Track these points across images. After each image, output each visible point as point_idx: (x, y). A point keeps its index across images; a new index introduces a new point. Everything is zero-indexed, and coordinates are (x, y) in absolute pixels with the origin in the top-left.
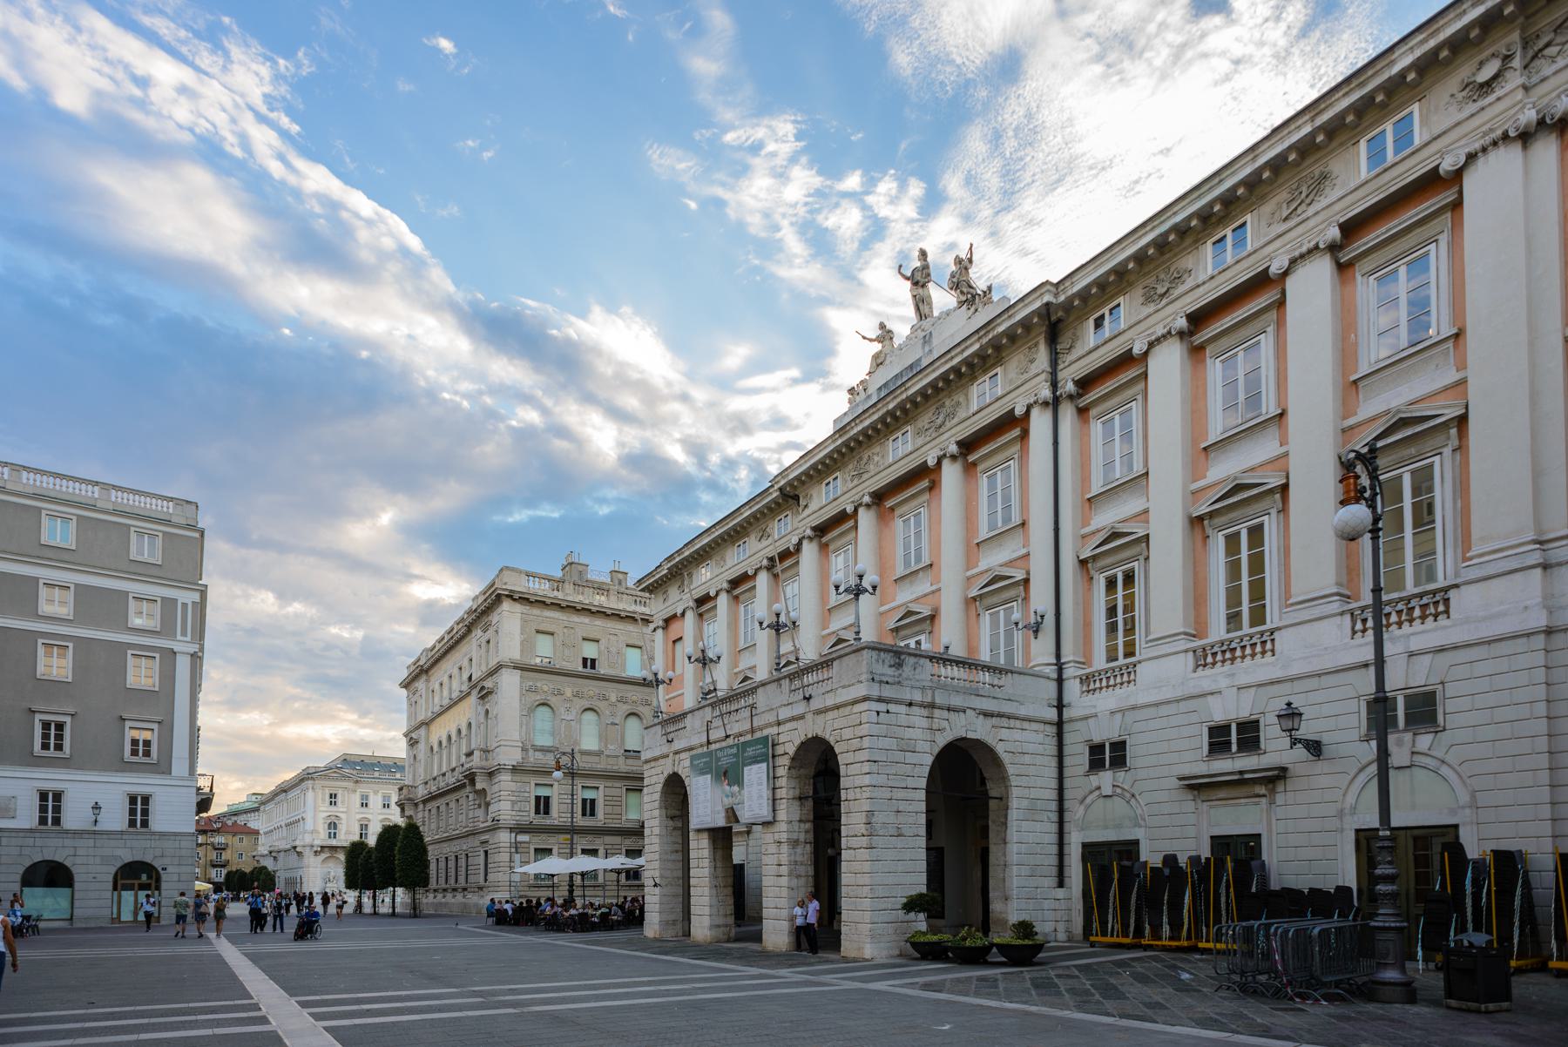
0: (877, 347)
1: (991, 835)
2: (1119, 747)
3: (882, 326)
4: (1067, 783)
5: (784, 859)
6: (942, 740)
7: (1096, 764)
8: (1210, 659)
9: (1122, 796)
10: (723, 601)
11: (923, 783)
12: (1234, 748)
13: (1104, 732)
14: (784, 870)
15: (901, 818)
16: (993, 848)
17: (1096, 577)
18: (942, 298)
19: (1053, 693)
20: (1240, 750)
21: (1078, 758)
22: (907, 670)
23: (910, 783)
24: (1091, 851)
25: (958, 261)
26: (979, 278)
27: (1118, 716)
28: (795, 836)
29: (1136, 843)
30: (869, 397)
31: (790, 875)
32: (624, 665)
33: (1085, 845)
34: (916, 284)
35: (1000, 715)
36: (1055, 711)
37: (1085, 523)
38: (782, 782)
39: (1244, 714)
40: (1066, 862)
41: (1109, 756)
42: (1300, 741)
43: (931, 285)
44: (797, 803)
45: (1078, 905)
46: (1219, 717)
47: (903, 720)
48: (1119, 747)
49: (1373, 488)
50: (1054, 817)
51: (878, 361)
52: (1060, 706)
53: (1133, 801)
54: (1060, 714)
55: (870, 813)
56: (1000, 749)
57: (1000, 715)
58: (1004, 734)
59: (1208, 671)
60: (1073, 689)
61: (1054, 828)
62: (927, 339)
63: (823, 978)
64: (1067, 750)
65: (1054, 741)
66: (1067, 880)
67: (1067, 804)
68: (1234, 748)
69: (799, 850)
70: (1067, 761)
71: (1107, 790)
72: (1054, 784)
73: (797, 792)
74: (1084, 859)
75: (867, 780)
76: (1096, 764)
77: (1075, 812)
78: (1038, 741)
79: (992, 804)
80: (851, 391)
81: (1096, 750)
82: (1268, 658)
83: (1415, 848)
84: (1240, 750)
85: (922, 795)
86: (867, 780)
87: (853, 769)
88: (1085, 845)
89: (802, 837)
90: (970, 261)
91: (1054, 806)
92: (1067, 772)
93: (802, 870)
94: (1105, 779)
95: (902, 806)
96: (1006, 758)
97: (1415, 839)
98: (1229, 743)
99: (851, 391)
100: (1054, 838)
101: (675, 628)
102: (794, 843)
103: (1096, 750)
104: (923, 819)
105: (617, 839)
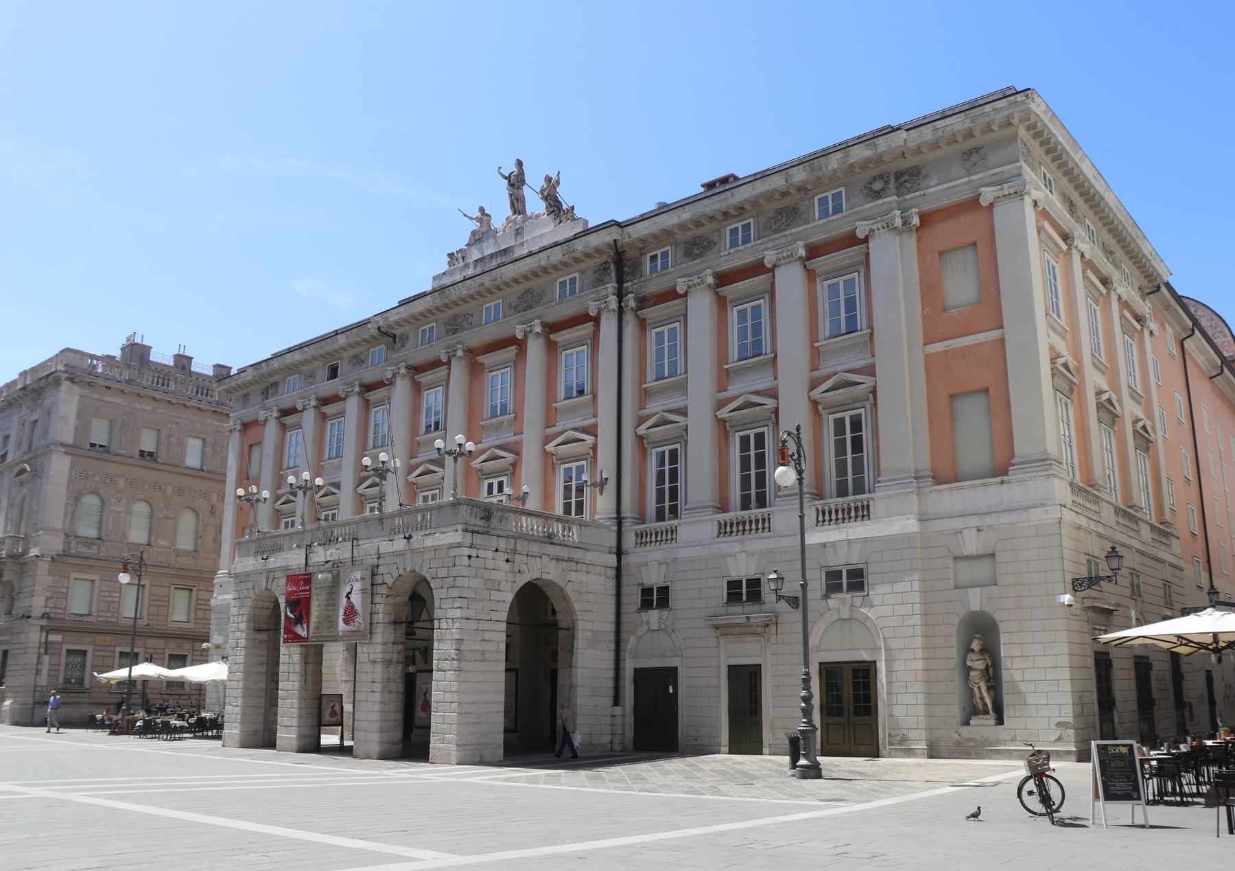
0: (475, 226)
1: (560, 659)
2: (664, 591)
3: (482, 210)
4: (624, 618)
5: (378, 677)
6: (521, 581)
7: (646, 604)
8: (728, 529)
9: (665, 631)
10: (309, 419)
11: (504, 617)
12: (744, 598)
13: (654, 578)
14: (377, 687)
15: (486, 646)
16: (561, 673)
17: (649, 451)
18: (535, 205)
19: (614, 543)
20: (748, 601)
21: (632, 599)
22: (494, 522)
23: (495, 616)
24: (639, 673)
25: (548, 179)
26: (566, 196)
27: (663, 567)
28: (389, 656)
29: (675, 670)
30: (467, 265)
31: (382, 692)
32: (183, 456)
33: (637, 671)
34: (511, 185)
35: (570, 560)
36: (614, 557)
37: (642, 407)
38: (380, 608)
39: (751, 574)
40: (621, 685)
41: (656, 598)
42: (783, 597)
43: (525, 188)
44: (392, 627)
45: (630, 720)
46: (735, 574)
47: (490, 564)
48: (664, 591)
49: (798, 452)
50: (612, 646)
51: (477, 239)
52: (619, 553)
53: (673, 636)
54: (619, 561)
55: (460, 641)
56: (569, 590)
57: (570, 560)
58: (573, 576)
59: (727, 538)
60: (629, 540)
61: (612, 655)
62: (518, 232)
63: (422, 776)
64: (624, 590)
65: (613, 583)
66: (621, 700)
67: (623, 635)
68: (744, 598)
69: (392, 668)
70: (624, 600)
71: (654, 626)
72: (612, 618)
73: (393, 617)
74: (636, 681)
75: (458, 613)
76: (646, 604)
77: (630, 643)
78: (602, 585)
79: (562, 634)
80: (451, 255)
81: (647, 592)
82: (766, 534)
83: (854, 677)
84: (748, 601)
85: (503, 626)
86: (458, 613)
87: (445, 604)
88: (637, 671)
89: (395, 657)
90: (558, 182)
91: (612, 637)
92: (624, 609)
93: (393, 686)
94: (653, 616)
95: (487, 636)
96: (572, 596)
97: (855, 672)
98: (741, 594)
99: (451, 255)
100: (611, 665)
101: (254, 432)
102: (387, 663)
103: (647, 592)
104: (503, 647)
105: (160, 643)
